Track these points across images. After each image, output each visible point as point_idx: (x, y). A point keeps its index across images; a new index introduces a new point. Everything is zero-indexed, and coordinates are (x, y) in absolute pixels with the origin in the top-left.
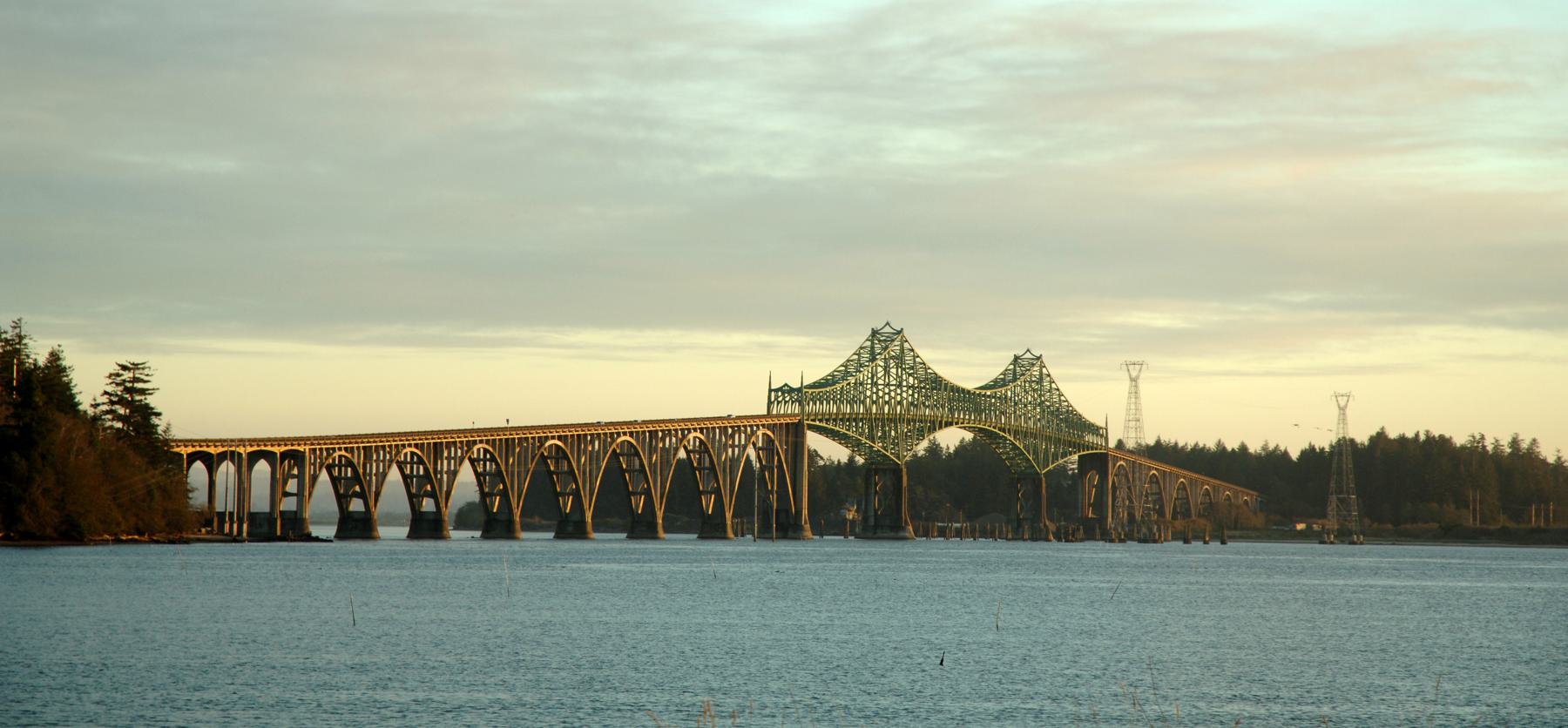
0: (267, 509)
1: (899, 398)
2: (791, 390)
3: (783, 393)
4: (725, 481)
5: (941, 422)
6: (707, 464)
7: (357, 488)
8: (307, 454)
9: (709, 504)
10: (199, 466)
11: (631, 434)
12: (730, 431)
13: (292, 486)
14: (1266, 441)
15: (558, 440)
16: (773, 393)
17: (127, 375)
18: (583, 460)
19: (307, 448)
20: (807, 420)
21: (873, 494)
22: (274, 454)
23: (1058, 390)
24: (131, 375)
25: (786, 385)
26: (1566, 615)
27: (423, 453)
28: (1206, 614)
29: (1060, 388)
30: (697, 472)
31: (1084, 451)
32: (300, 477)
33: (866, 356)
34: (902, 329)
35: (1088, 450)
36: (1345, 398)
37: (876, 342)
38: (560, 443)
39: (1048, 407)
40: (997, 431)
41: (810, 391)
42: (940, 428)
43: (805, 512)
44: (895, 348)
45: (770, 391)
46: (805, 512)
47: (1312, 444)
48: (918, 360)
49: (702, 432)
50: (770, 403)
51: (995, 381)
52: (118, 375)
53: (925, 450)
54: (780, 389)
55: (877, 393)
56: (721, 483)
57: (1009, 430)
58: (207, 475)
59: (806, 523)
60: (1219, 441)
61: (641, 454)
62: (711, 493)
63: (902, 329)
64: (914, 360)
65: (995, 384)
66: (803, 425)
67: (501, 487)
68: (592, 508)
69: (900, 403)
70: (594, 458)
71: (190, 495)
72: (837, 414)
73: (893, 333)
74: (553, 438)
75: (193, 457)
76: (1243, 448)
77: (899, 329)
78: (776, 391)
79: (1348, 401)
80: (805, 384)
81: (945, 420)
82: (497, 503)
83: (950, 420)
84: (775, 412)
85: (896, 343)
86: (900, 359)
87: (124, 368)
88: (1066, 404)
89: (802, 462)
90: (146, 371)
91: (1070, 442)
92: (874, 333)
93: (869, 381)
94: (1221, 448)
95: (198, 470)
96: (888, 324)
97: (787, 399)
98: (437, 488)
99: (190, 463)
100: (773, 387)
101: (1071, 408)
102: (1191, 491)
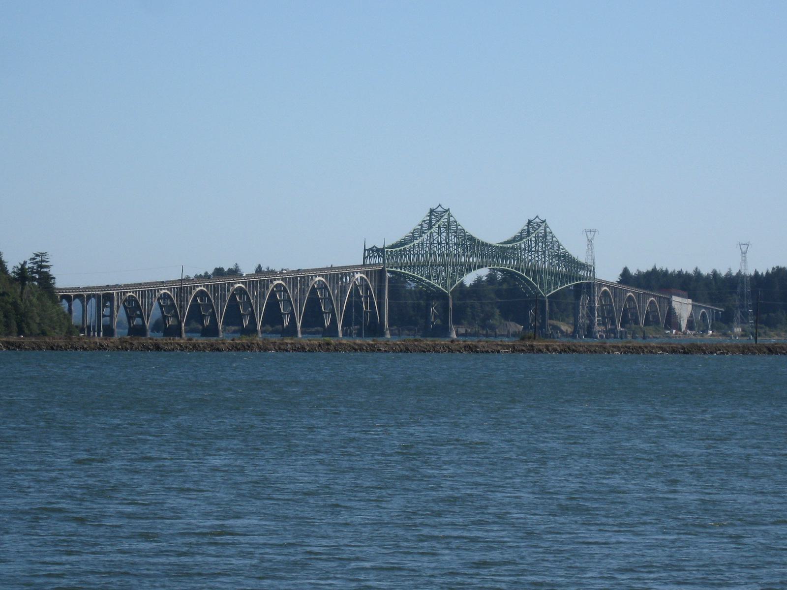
0: (80, 323)
1: (530, 258)
2: (378, 250)
3: (373, 252)
4: (337, 307)
5: (475, 266)
7: (138, 313)
10: (64, 301)
11: (323, 276)
12: (340, 276)
13: (106, 311)
17: (39, 259)
19: (115, 292)
22: (82, 295)
23: (558, 242)
24: (40, 259)
26: (785, 434)
27: (171, 292)
28: (256, 422)
29: (559, 240)
31: (577, 281)
32: (112, 307)
33: (426, 226)
34: (449, 209)
35: (580, 281)
36: (746, 246)
37: (433, 217)
39: (552, 253)
40: (514, 270)
41: (390, 250)
42: (475, 269)
43: (386, 323)
44: (444, 220)
45: (365, 250)
46: (386, 323)
47: (757, 270)
48: (459, 227)
49: (323, 277)
50: (364, 258)
51: (515, 238)
52: (34, 259)
53: (487, 276)
54: (371, 249)
55: (544, 258)
58: (81, 305)
60: (697, 269)
62: (329, 313)
63: (449, 209)
64: (457, 227)
65: (514, 240)
67: (250, 309)
69: (531, 260)
72: (407, 263)
75: (63, 297)
76: (715, 273)
78: (369, 250)
80: (386, 246)
83: (481, 264)
84: (368, 263)
85: (541, 228)
86: (448, 227)
87: (37, 255)
89: (385, 294)
90: (47, 257)
92: (432, 211)
93: (533, 249)
95: (77, 304)
97: (375, 255)
98: (178, 312)
99: (61, 301)
100: (366, 248)
102: (660, 306)
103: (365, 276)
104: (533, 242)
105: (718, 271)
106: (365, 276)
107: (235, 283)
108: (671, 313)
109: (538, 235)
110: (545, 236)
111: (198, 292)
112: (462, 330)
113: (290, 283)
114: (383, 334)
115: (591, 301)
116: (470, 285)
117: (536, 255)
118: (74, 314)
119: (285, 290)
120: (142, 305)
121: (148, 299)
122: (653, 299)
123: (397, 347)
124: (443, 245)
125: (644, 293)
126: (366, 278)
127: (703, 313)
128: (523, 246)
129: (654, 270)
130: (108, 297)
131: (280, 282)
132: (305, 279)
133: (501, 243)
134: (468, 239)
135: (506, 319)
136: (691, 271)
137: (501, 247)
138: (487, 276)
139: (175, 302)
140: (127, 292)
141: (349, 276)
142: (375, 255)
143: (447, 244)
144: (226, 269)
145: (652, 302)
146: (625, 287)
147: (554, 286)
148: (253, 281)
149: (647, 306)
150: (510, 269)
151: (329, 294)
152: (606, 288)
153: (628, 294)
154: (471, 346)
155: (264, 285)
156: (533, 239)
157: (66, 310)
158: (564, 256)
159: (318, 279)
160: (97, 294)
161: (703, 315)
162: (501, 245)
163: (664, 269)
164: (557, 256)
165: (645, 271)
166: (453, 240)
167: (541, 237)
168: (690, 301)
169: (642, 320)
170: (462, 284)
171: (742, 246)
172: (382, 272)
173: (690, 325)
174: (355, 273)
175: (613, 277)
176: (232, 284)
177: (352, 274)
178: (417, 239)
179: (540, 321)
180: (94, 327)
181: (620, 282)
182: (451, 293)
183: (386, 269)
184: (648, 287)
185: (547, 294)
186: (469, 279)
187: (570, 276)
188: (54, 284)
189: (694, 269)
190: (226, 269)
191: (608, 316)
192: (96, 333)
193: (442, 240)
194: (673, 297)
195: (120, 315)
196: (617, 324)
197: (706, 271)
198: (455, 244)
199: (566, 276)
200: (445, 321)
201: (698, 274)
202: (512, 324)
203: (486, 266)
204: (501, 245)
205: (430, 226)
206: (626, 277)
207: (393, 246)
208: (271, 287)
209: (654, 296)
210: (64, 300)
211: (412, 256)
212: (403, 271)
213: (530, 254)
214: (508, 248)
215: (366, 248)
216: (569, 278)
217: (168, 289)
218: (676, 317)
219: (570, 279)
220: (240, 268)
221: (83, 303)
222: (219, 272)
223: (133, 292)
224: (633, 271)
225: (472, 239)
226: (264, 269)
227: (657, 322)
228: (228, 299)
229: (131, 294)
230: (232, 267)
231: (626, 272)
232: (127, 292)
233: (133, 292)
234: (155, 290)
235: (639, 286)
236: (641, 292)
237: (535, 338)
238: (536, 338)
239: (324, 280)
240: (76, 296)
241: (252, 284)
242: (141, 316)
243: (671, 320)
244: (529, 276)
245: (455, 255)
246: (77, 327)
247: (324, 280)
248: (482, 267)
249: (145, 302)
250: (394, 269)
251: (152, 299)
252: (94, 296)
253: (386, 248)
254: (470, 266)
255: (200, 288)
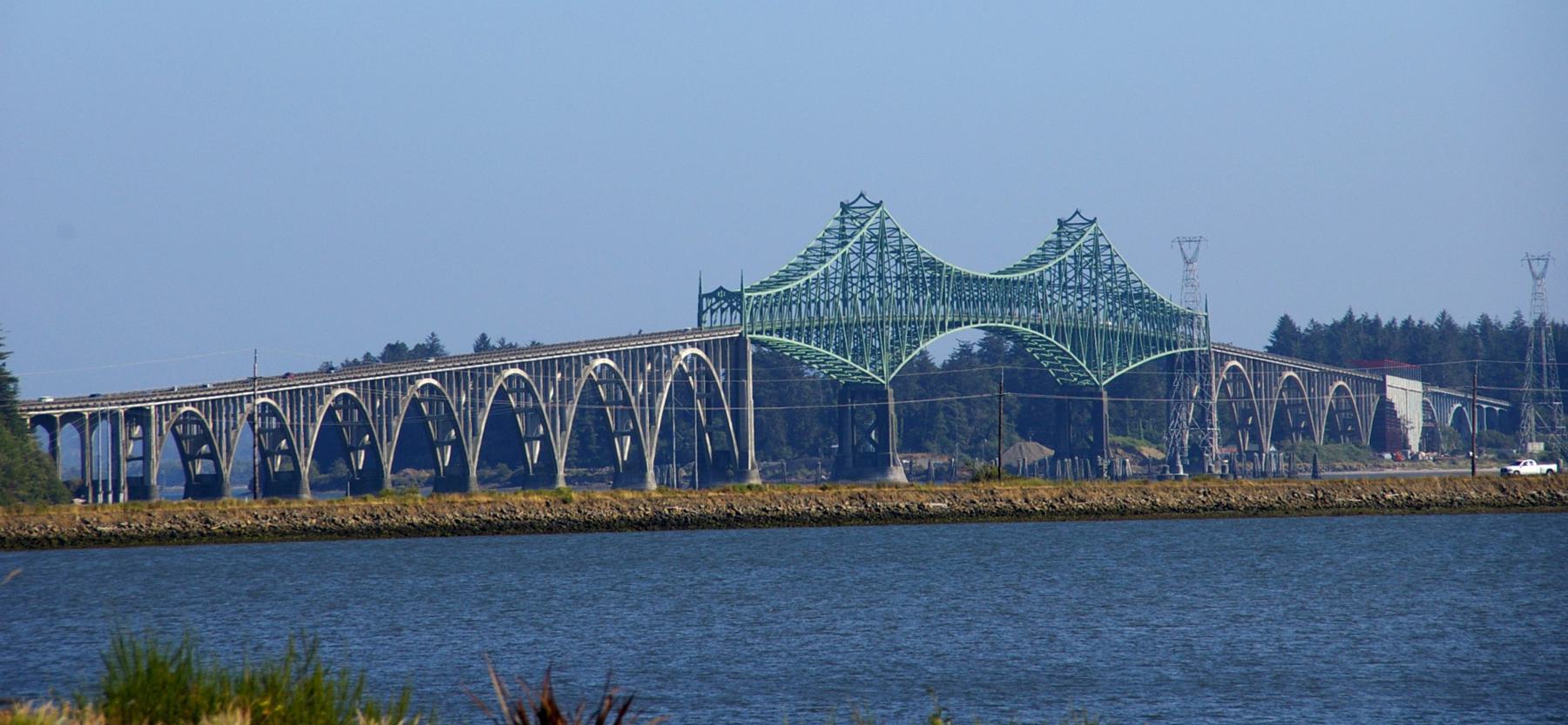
5: (943, 323)
6: (621, 397)
8: (153, 412)
9: (624, 449)
10: (41, 431)
11: (610, 355)
14: (1518, 312)
15: (433, 378)
16: (704, 299)
18: (551, 394)
19: (153, 404)
20: (751, 333)
21: (850, 425)
22: (80, 415)
25: (721, 288)
27: (278, 403)
30: (430, 423)
32: (145, 437)
36: (1542, 263)
38: (435, 382)
39: (1111, 289)
40: (1029, 330)
42: (943, 329)
43: (752, 453)
45: (701, 297)
46: (752, 453)
49: (611, 358)
50: (701, 313)
53: (980, 345)
56: (639, 421)
57: (1048, 327)
59: (753, 467)
60: (1444, 314)
61: (535, 389)
64: (900, 241)
65: (1030, 263)
66: (746, 341)
68: (477, 459)
69: (1065, 308)
70: (565, 391)
71: (1271, 344)
73: (1083, 224)
74: (513, 366)
75: (36, 420)
76: (1485, 323)
77: (1092, 219)
78: (709, 296)
79: (1546, 266)
81: (949, 319)
82: (362, 458)
85: (1086, 237)
88: (1138, 284)
91: (1147, 337)
94: (1447, 318)
96: (1077, 212)
99: (33, 430)
100: (703, 293)
101: (1146, 291)
103: (701, 353)
104: (1069, 268)
105: (1492, 318)
106: (701, 353)
107: (505, 367)
108: (1386, 410)
109: (1080, 251)
110: (1096, 254)
111: (336, 399)
112: (922, 461)
113: (537, 373)
114: (742, 474)
115: (1205, 393)
116: (944, 365)
117: (1079, 296)
118: (62, 455)
119: (528, 389)
120: (292, 426)
121: (227, 418)
122: (1341, 383)
123: (710, 502)
124: (872, 280)
125: (1322, 372)
126: (704, 356)
127: (1459, 412)
128: (1047, 277)
129: (1349, 318)
130: (138, 416)
131: (518, 371)
132: (571, 364)
133: (999, 273)
134: (926, 264)
135: (1025, 437)
136: (1431, 320)
137: (999, 281)
138: (980, 345)
139: (288, 422)
140: (180, 405)
141: (668, 354)
142: (725, 306)
143: (881, 277)
144: (411, 347)
145: (1340, 390)
146: (1278, 360)
147: (1134, 355)
148: (457, 373)
149: (1329, 399)
150: (1020, 327)
151: (625, 393)
152: (1235, 363)
153: (1286, 374)
154: (864, 495)
155: (481, 379)
156: (1071, 261)
157: (45, 448)
158: (1139, 296)
159: (599, 362)
160: (111, 411)
161: (1459, 414)
162: (1000, 277)
163: (1371, 317)
164: (1124, 295)
165: (1330, 323)
166: (892, 268)
167: (1087, 255)
168: (1417, 385)
169: (1320, 434)
170: (923, 362)
171: (1534, 263)
172: (739, 343)
173: (1430, 438)
174: (681, 347)
175: (1256, 338)
176: (412, 380)
177: (672, 349)
178: (813, 269)
179: (1091, 438)
180: (105, 482)
181: (1270, 350)
182: (893, 382)
183: (748, 336)
184: (1334, 359)
185: (1106, 377)
186: (940, 348)
187: (1161, 341)
188: (14, 393)
189: (1437, 314)
190: (411, 347)
191: (1238, 423)
192: (110, 496)
193: (870, 269)
194: (1388, 377)
195: (164, 455)
196: (1264, 441)
197: (1465, 318)
198: (898, 278)
199: (1146, 339)
200: (883, 443)
201: (1446, 325)
202: (1033, 446)
203: (967, 323)
204: (1000, 277)
205: (843, 239)
206: (1286, 338)
207: (764, 286)
208: (498, 382)
209: (1345, 377)
210: (39, 427)
211: (803, 306)
212: (784, 340)
213: (1064, 294)
214: (1015, 282)
215: (703, 293)
216: (1145, 344)
217: (270, 395)
218: (1397, 422)
219: (1154, 344)
220: (441, 343)
221: (81, 430)
222: (395, 353)
223: (193, 404)
224: (1302, 324)
225: (932, 264)
226: (494, 342)
227: (1355, 435)
228: (403, 410)
229: (190, 408)
230: (423, 340)
231: (1285, 324)
232: (180, 405)
233: (193, 404)
234: (241, 398)
235: (1311, 357)
236: (1315, 368)
237: (999, 477)
238: (1002, 477)
239: (612, 364)
240: (66, 418)
241: (457, 379)
242: (212, 456)
243: (1387, 431)
244: (1064, 342)
245: (899, 302)
246: (67, 484)
247: (612, 364)
248: (958, 324)
249: (221, 423)
250: (764, 337)
251: (235, 419)
252: (104, 415)
253: (747, 291)
254: (932, 323)
255: (340, 391)
